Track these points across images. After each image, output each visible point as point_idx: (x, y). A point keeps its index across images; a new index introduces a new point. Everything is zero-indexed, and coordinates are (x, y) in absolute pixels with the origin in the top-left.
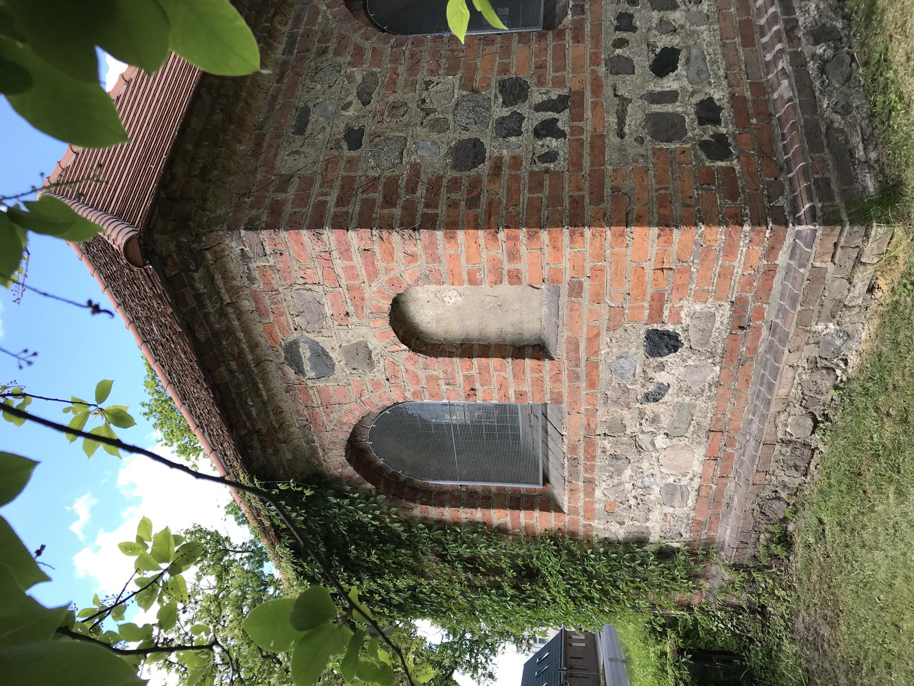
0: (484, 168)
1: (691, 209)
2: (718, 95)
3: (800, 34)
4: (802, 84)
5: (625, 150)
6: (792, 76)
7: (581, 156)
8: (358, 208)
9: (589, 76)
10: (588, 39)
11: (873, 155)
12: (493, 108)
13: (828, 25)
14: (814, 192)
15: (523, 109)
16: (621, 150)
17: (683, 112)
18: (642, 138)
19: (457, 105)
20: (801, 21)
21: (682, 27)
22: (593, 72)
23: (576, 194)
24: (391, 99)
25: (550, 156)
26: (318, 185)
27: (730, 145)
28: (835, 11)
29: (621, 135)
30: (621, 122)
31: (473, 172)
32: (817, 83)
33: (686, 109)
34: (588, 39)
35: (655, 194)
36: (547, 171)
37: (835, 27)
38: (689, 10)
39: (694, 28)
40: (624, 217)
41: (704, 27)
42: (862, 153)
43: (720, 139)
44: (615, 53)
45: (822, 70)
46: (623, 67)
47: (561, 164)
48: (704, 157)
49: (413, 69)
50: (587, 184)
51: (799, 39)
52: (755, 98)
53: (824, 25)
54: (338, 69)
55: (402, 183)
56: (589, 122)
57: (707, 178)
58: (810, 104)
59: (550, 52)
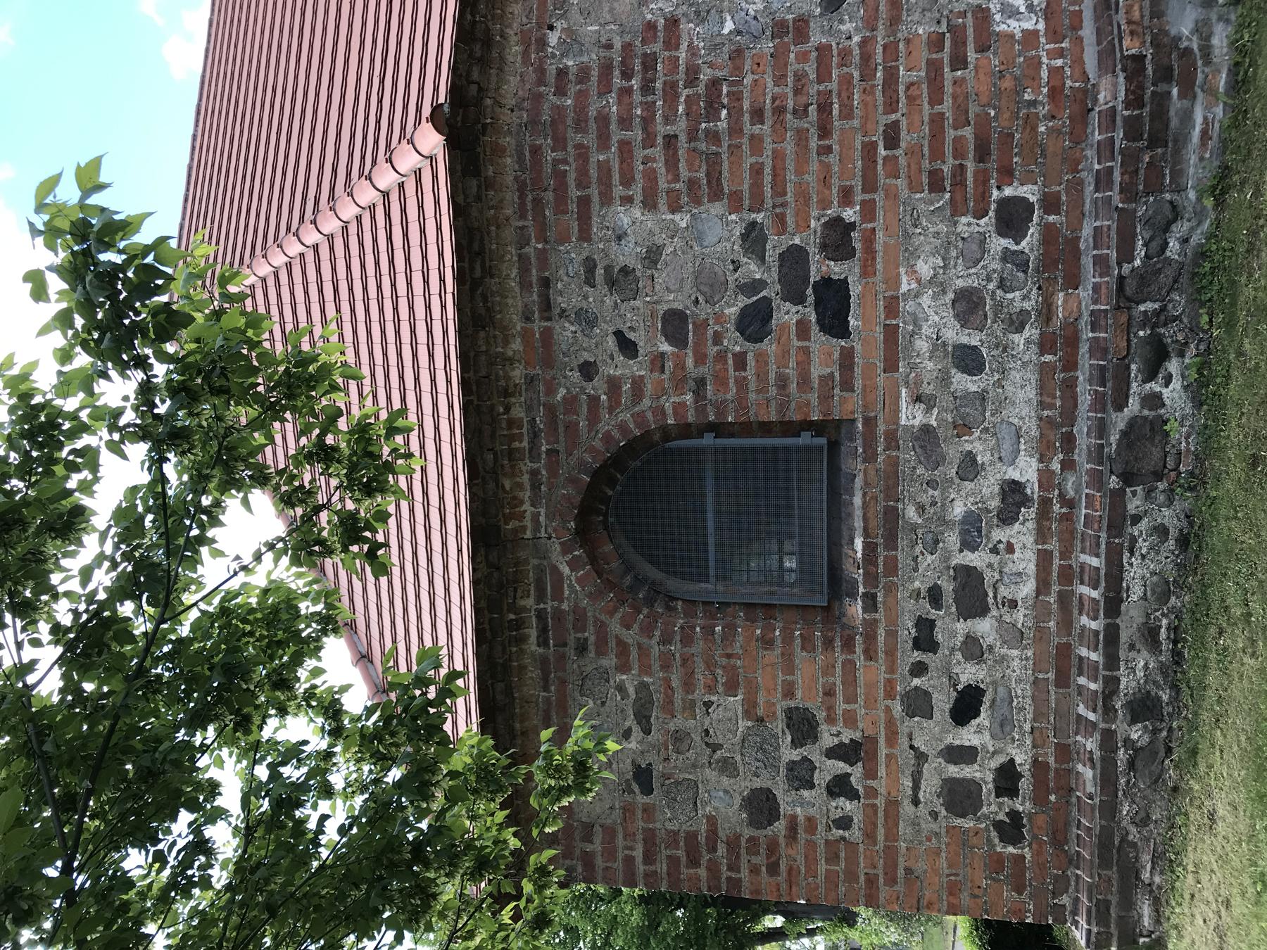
0: (780, 826)
1: (978, 900)
2: (1021, 758)
3: (1118, 705)
4: (1107, 779)
5: (919, 824)
6: (1098, 766)
7: (875, 825)
8: (665, 867)
9: (882, 715)
10: (881, 656)
11: (1157, 879)
12: (782, 750)
13: (1153, 693)
14: (1093, 914)
15: (813, 753)
16: (915, 823)
17: (981, 779)
18: (936, 812)
19: (743, 741)
20: (1124, 681)
21: (991, 648)
22: (888, 707)
23: (872, 872)
24: (672, 727)
25: (844, 822)
26: (620, 836)
27: (1024, 826)
28: (1165, 674)
29: (916, 802)
30: (916, 787)
31: (769, 831)
32: (1123, 781)
33: (982, 773)
34: (881, 656)
35: (945, 880)
36: (843, 838)
37: (1159, 698)
38: (1001, 616)
39: (1004, 651)
40: (915, 902)
41: (1015, 652)
42: (1148, 875)
43: (1014, 815)
44: (912, 684)
45: (1131, 764)
46: (919, 704)
47: (855, 834)
48: (996, 841)
49: (688, 685)
50: (881, 861)
51: (1116, 711)
52: (1058, 766)
53: (1148, 692)
54: (604, 675)
55: (702, 839)
56: (883, 782)
57: (996, 863)
58: (1109, 809)
59: (839, 670)
